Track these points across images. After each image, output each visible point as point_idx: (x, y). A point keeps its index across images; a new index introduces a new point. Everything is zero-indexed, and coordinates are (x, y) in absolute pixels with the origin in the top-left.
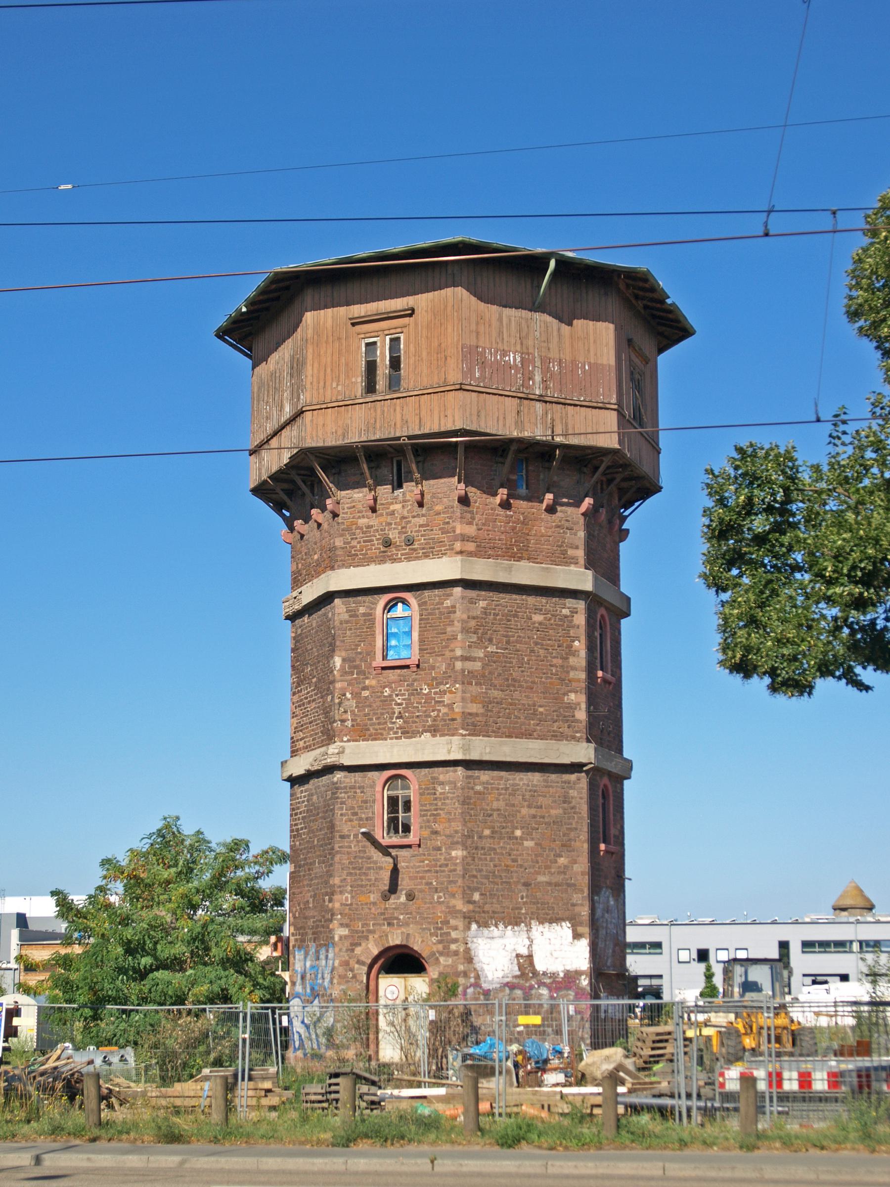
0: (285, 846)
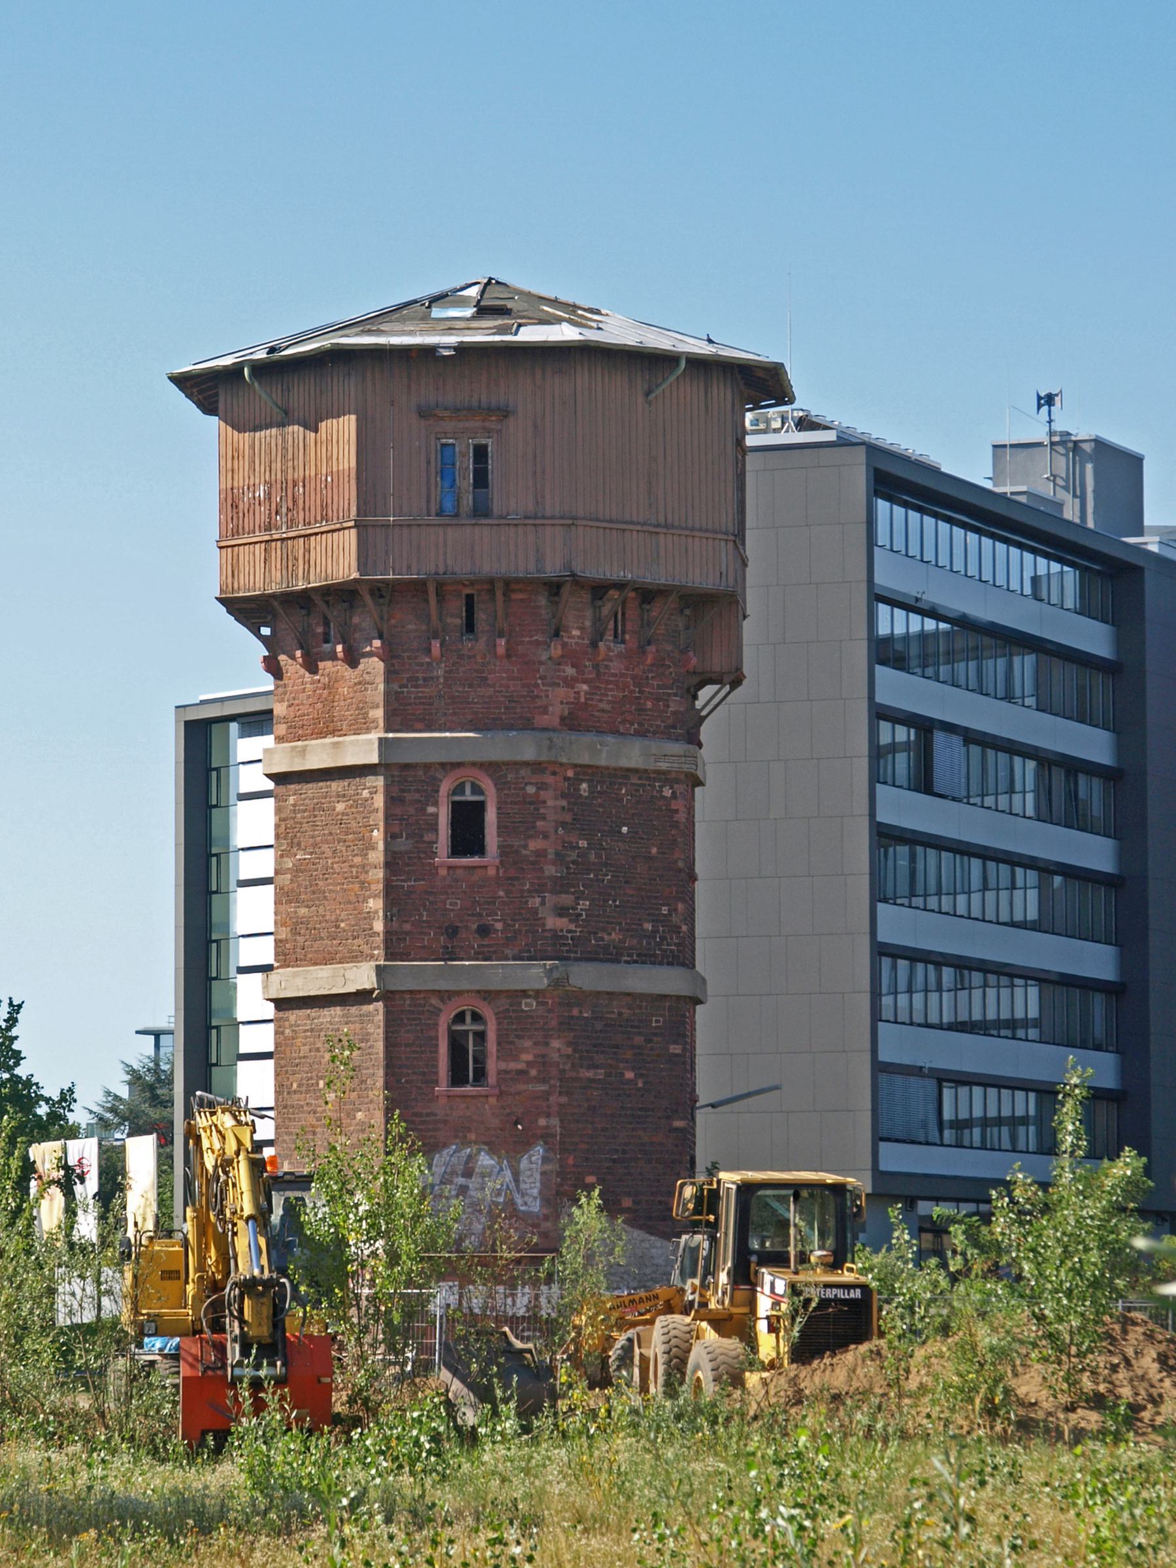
0: (271, 1103)
